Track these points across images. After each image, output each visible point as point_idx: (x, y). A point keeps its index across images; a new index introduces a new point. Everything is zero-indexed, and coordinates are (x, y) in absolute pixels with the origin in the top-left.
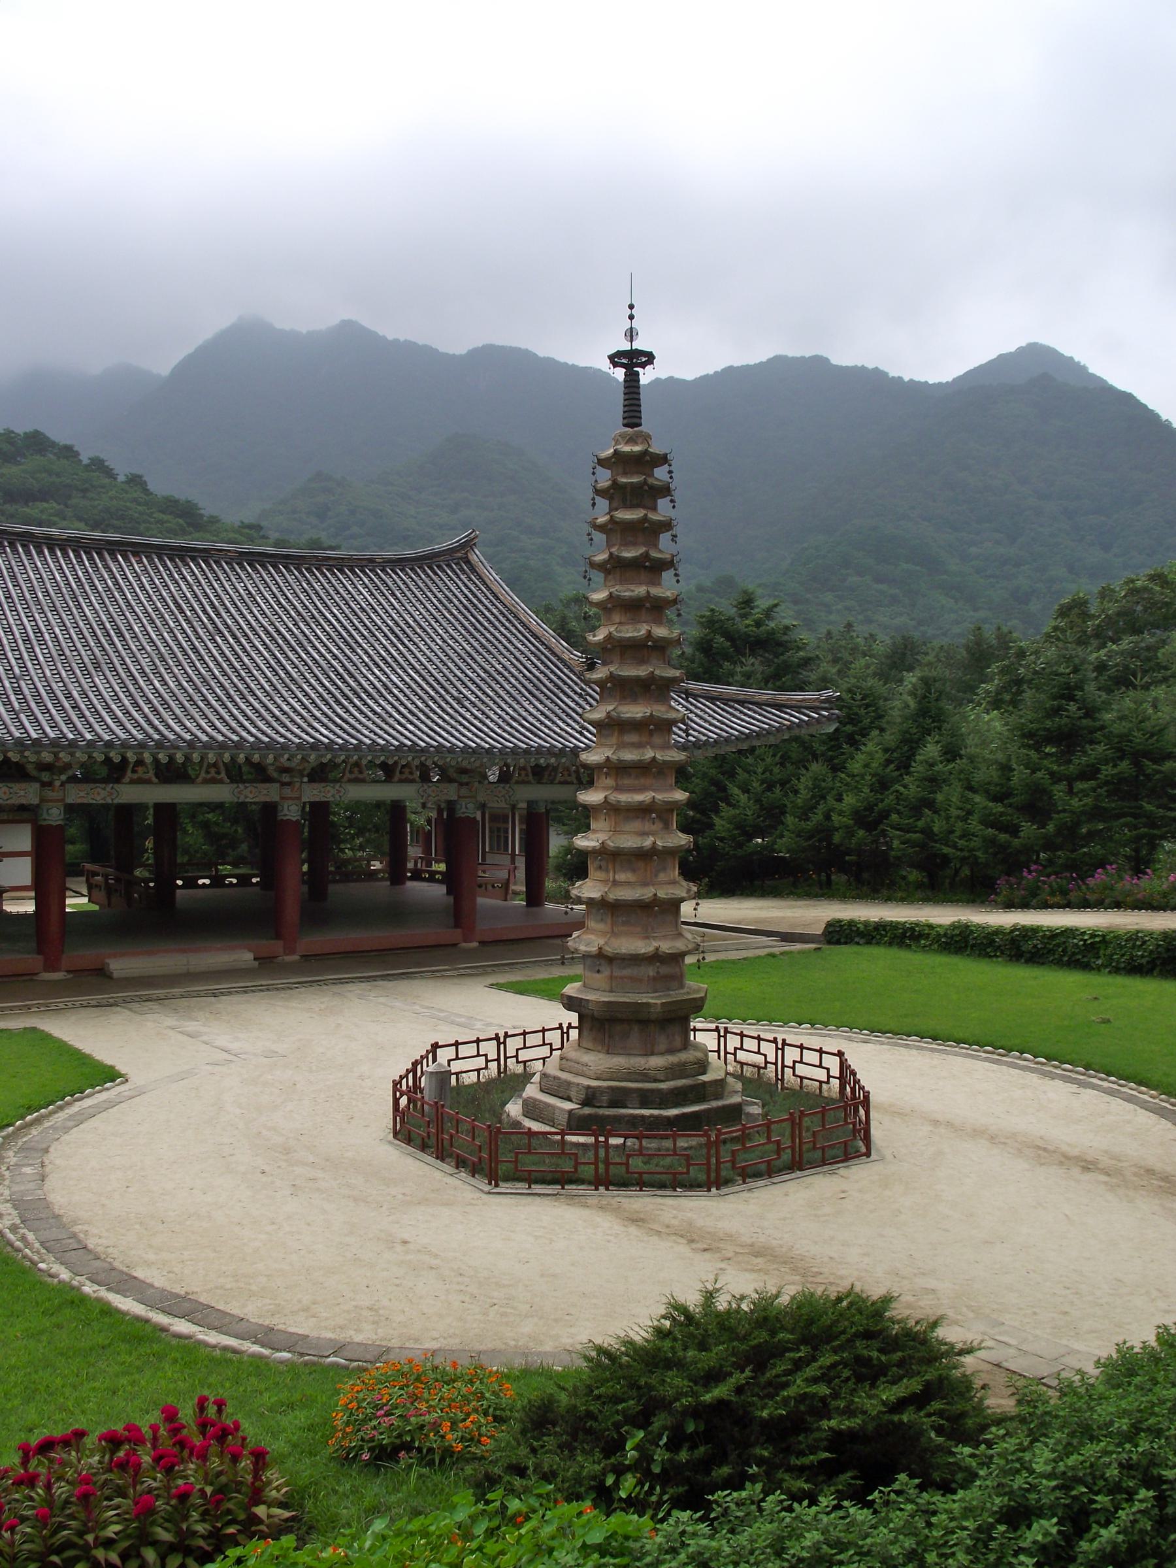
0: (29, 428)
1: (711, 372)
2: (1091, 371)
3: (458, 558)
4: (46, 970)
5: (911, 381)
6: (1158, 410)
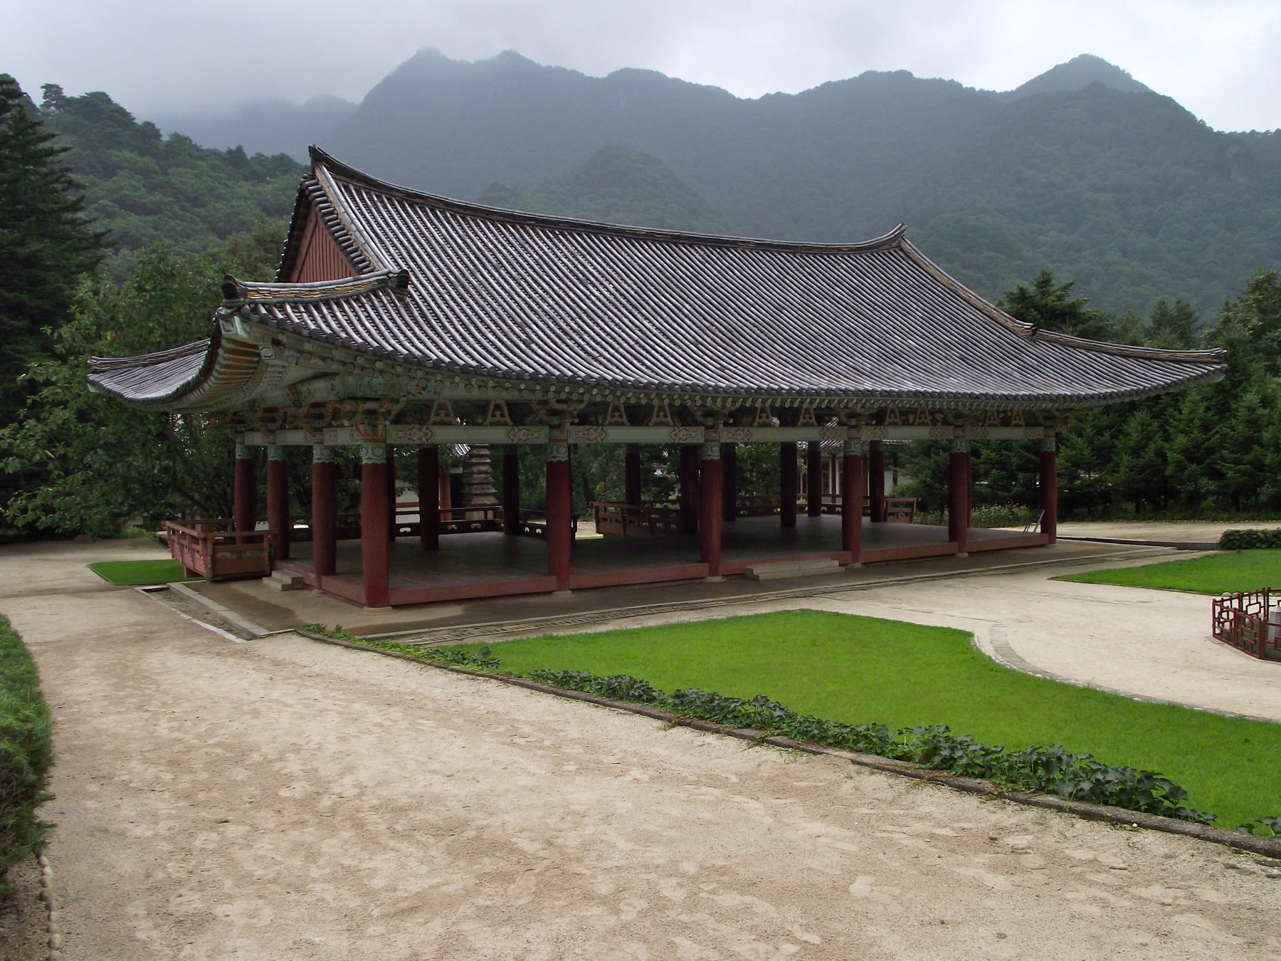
0: (277, 153)
1: (812, 87)
2: (1134, 78)
3: (893, 246)
4: (711, 575)
5: (982, 91)
6: (1194, 112)
